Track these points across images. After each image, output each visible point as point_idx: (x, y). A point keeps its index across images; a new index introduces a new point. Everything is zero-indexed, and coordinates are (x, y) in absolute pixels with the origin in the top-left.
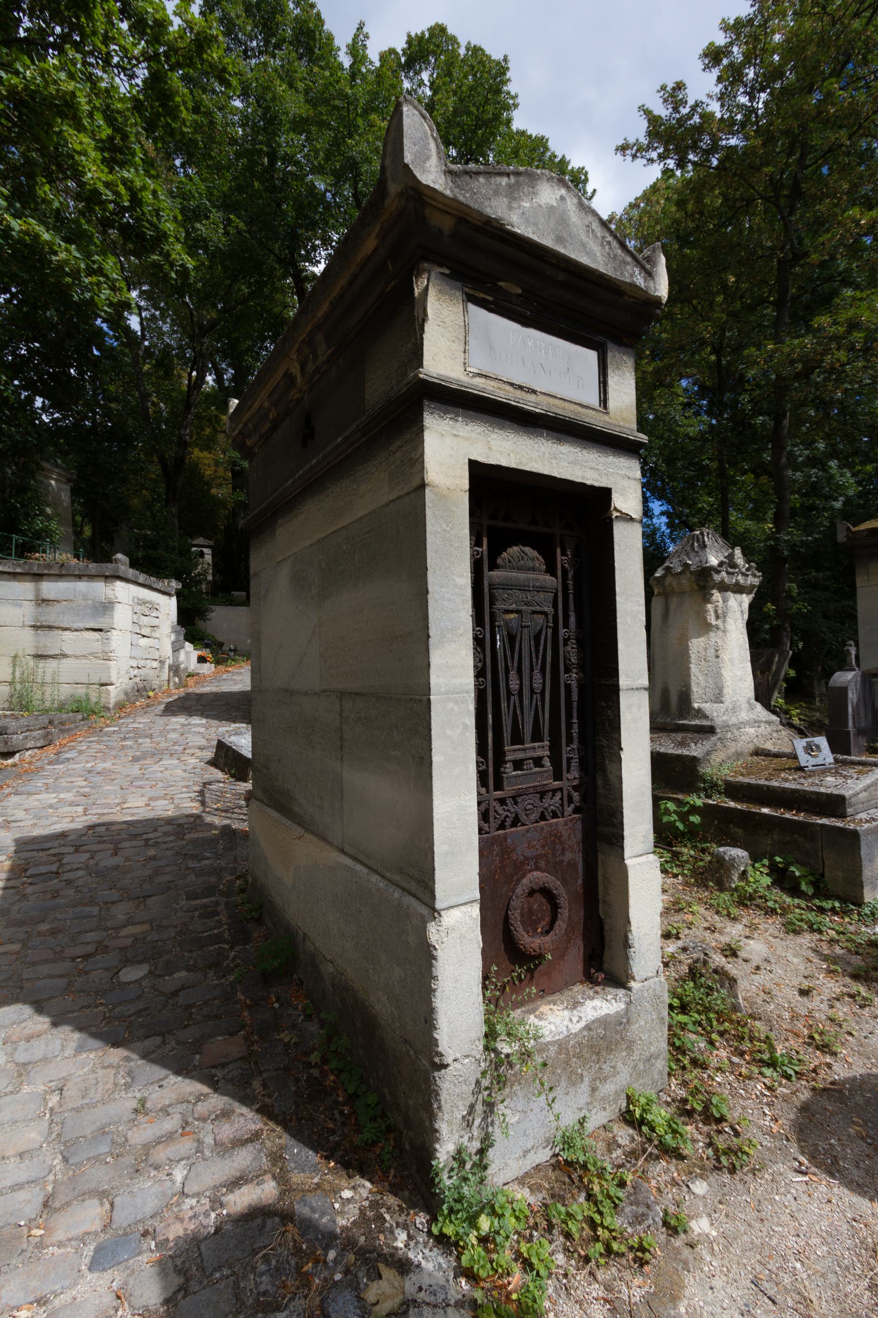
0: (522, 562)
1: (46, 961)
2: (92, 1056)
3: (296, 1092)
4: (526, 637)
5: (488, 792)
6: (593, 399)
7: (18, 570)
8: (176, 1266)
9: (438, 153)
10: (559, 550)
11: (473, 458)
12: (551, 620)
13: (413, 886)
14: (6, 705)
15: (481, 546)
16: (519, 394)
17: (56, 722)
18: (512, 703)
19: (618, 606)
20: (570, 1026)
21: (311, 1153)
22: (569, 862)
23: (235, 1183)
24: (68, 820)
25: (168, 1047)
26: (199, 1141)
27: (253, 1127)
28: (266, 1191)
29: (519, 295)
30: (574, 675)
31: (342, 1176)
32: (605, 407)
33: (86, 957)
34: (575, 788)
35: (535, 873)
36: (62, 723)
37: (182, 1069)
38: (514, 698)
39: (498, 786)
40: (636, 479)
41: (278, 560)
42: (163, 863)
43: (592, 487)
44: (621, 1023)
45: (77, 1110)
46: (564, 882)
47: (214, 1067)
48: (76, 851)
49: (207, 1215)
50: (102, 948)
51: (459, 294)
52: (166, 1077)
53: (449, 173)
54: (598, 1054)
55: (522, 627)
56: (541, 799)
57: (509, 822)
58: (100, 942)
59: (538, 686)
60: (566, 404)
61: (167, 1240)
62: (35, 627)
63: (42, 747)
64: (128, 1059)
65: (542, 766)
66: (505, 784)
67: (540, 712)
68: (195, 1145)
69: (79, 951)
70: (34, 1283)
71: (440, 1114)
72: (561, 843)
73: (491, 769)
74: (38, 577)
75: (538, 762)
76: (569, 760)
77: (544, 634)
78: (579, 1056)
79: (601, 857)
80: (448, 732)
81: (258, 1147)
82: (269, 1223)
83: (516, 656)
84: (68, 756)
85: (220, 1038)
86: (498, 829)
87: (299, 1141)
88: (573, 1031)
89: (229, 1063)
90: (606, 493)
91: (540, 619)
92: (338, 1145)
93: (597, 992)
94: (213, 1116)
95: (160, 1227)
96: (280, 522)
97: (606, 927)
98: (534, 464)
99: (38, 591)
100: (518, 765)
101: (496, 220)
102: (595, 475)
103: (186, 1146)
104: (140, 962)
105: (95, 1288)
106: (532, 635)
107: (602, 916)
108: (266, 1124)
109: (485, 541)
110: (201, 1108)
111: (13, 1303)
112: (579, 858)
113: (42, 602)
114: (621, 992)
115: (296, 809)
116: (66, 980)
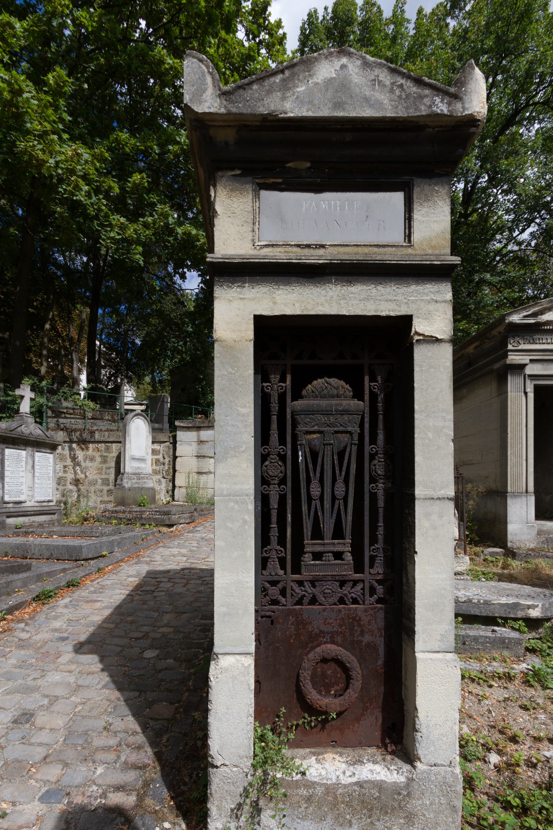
0: (326, 391)
1: (120, 637)
2: (107, 692)
3: (181, 751)
4: (328, 453)
5: (285, 574)
6: (398, 237)
7: (190, 425)
8: (67, 818)
10: (367, 379)
11: (258, 313)
14: (185, 500)
15: (285, 382)
16: (306, 251)
17: (198, 510)
18: (336, 507)
19: (417, 423)
20: (341, 777)
21: (166, 790)
23: (119, 788)
24: (176, 564)
25: (140, 699)
26: (119, 757)
27: (147, 761)
28: (127, 800)
29: (309, 168)
30: (381, 485)
31: (172, 813)
32: (410, 241)
33: (137, 639)
34: (379, 582)
35: (329, 646)
36: (202, 511)
37: (137, 715)
39: (296, 569)
40: (445, 302)
42: (202, 595)
43: (389, 318)
44: (399, 794)
45: (83, 717)
46: (361, 660)
47: (151, 719)
48: (169, 581)
49: (96, 799)
50: (146, 636)
51: (249, 187)
52: (128, 716)
53: (224, 94)
54: (371, 810)
55: (324, 445)
56: (341, 586)
57: (306, 600)
58: (147, 633)
60: (360, 249)
61: (73, 802)
62: (197, 456)
63: (189, 523)
64: (118, 699)
66: (303, 569)
67: (343, 515)
68: (116, 758)
69: (135, 635)
70: (16, 794)
71: (211, 799)
72: (360, 625)
73: (289, 557)
74: (199, 428)
75: (338, 555)
76: (373, 559)
77: (348, 450)
78: (348, 805)
80: (228, 524)
81: (141, 773)
82: (119, 819)
84: (198, 529)
85: (165, 704)
86: (295, 605)
87: (164, 780)
88: (343, 782)
89: (159, 720)
90: (407, 320)
91: (345, 438)
92: (183, 793)
93: (384, 760)
94: (133, 746)
95: (73, 794)
98: (320, 308)
99: (199, 436)
100: (317, 556)
101: (269, 114)
102: (393, 306)
103: (111, 756)
104: (157, 649)
105: (32, 809)
106: (336, 451)
108: (154, 762)
109: (289, 378)
110: (131, 739)
111: (5, 798)
112: (380, 643)
113: (201, 442)
114: (406, 767)
116: (120, 649)
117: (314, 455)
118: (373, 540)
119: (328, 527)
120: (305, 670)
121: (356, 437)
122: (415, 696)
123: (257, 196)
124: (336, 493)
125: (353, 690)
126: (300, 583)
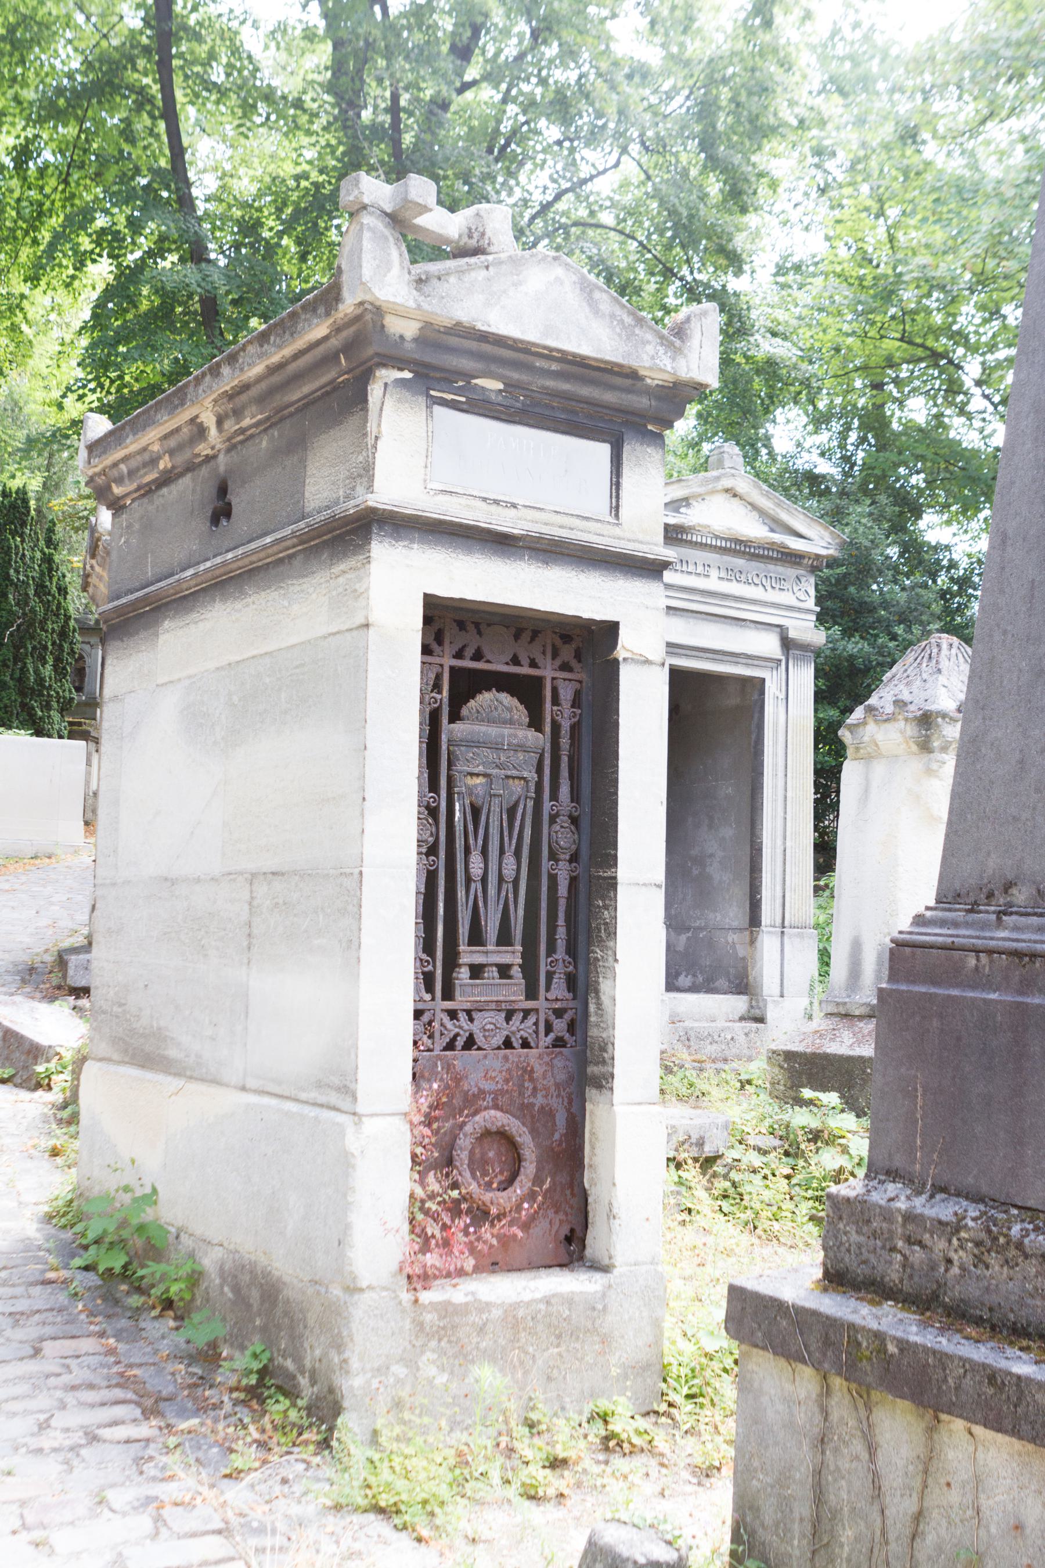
0: (495, 714)
4: (495, 809)
5: (433, 999)
9: (401, 263)
12: (533, 788)
13: (333, 1098)
15: (440, 692)
18: (503, 894)
22: (542, 1107)
32: (617, 516)
35: (493, 1112)
38: (476, 886)
39: (448, 994)
41: (160, 681)
44: (594, 1309)
46: (534, 1132)
54: (559, 1337)
56: (508, 1019)
57: (460, 1042)
59: (509, 872)
65: (510, 977)
66: (457, 993)
71: (350, 1345)
72: (531, 1079)
73: (439, 972)
75: (504, 971)
76: (550, 976)
77: (521, 806)
79: (589, 1106)
83: (481, 832)
90: (612, 628)
91: (517, 787)
96: (167, 624)
97: (590, 1200)
100: (476, 971)
106: (505, 807)
107: (587, 1186)
115: (172, 1053)
117: (476, 811)
118: (551, 950)
119: (491, 928)
120: (461, 1149)
121: (532, 787)
122: (613, 1166)
123: (430, 415)
124: (504, 872)
125: (527, 1176)
126: (453, 1014)
